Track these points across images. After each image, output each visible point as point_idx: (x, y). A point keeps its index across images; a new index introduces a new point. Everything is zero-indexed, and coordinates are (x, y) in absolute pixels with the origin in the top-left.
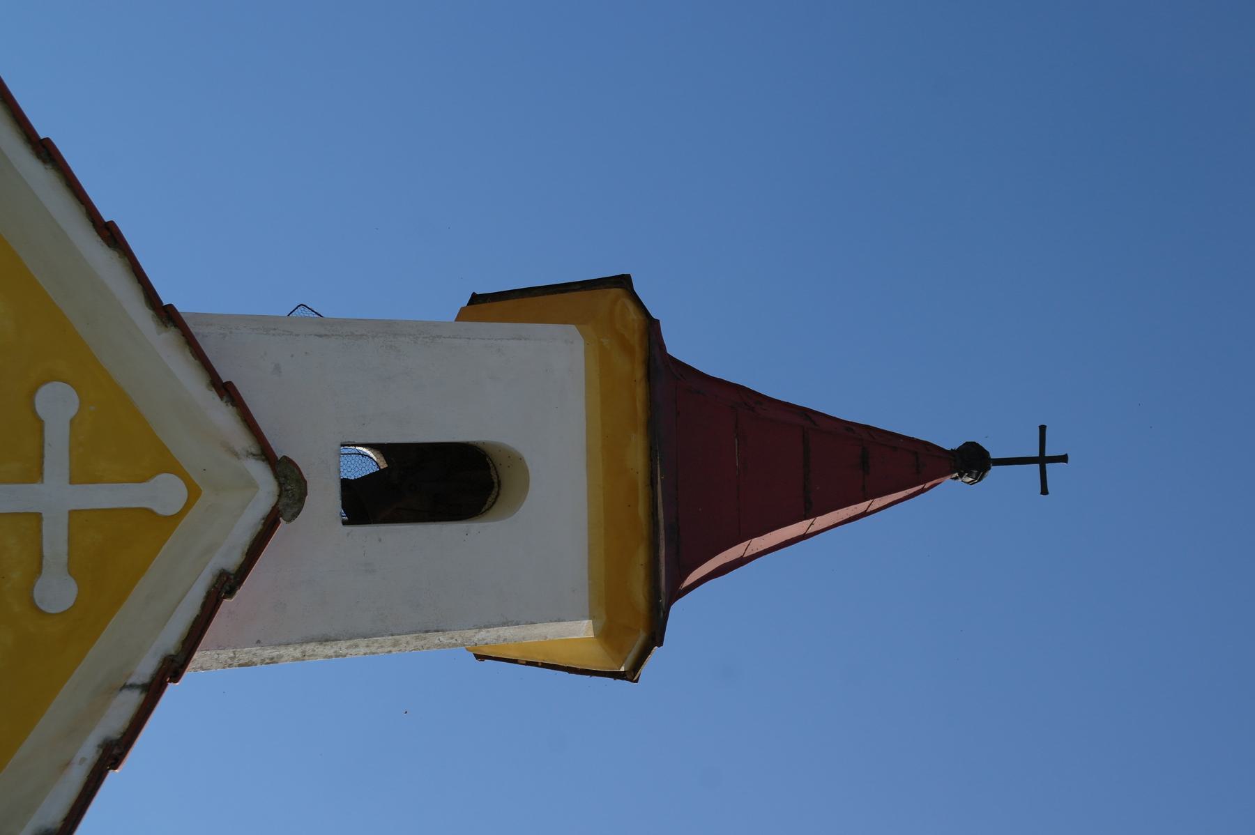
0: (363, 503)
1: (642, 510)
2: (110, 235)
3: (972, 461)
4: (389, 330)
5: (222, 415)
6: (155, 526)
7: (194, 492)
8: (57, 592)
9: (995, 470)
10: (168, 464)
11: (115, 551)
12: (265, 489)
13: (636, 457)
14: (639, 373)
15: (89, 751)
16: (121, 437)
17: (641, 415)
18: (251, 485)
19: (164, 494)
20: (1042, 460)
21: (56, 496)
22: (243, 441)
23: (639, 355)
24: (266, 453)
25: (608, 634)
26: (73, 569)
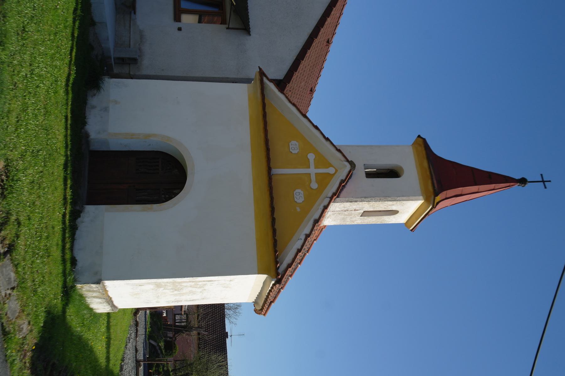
0: (369, 175)
1: (428, 173)
2: (316, 127)
3: (523, 181)
4: (371, 146)
5: (339, 155)
6: (331, 176)
7: (336, 171)
8: (314, 185)
9: (529, 184)
10: (330, 165)
11: (324, 179)
12: (348, 167)
13: (426, 164)
14: (423, 149)
15: (321, 207)
16: (322, 161)
17: (425, 156)
18: (346, 166)
19: (331, 170)
20: (543, 181)
21: (313, 171)
22: (343, 159)
23: (423, 146)
24: (347, 161)
25: (427, 200)
26: (316, 182)
